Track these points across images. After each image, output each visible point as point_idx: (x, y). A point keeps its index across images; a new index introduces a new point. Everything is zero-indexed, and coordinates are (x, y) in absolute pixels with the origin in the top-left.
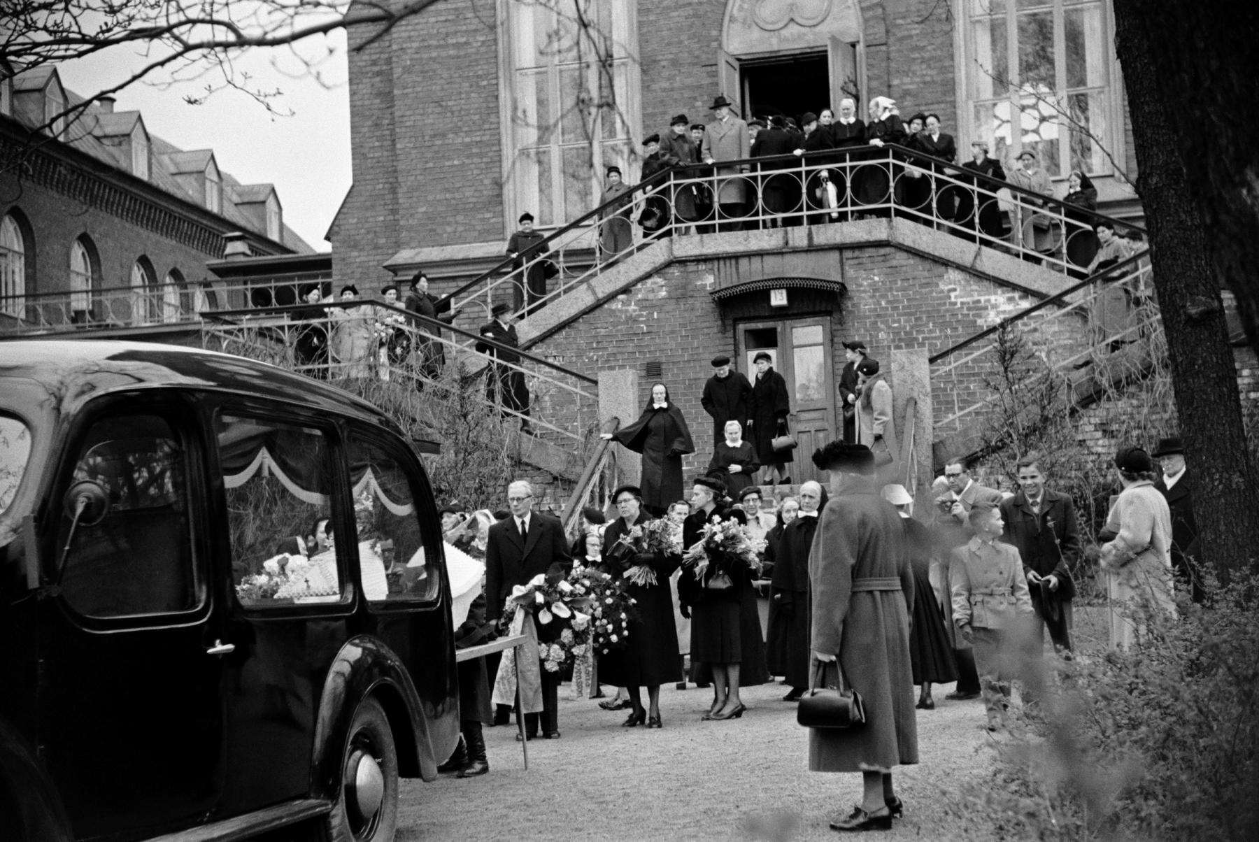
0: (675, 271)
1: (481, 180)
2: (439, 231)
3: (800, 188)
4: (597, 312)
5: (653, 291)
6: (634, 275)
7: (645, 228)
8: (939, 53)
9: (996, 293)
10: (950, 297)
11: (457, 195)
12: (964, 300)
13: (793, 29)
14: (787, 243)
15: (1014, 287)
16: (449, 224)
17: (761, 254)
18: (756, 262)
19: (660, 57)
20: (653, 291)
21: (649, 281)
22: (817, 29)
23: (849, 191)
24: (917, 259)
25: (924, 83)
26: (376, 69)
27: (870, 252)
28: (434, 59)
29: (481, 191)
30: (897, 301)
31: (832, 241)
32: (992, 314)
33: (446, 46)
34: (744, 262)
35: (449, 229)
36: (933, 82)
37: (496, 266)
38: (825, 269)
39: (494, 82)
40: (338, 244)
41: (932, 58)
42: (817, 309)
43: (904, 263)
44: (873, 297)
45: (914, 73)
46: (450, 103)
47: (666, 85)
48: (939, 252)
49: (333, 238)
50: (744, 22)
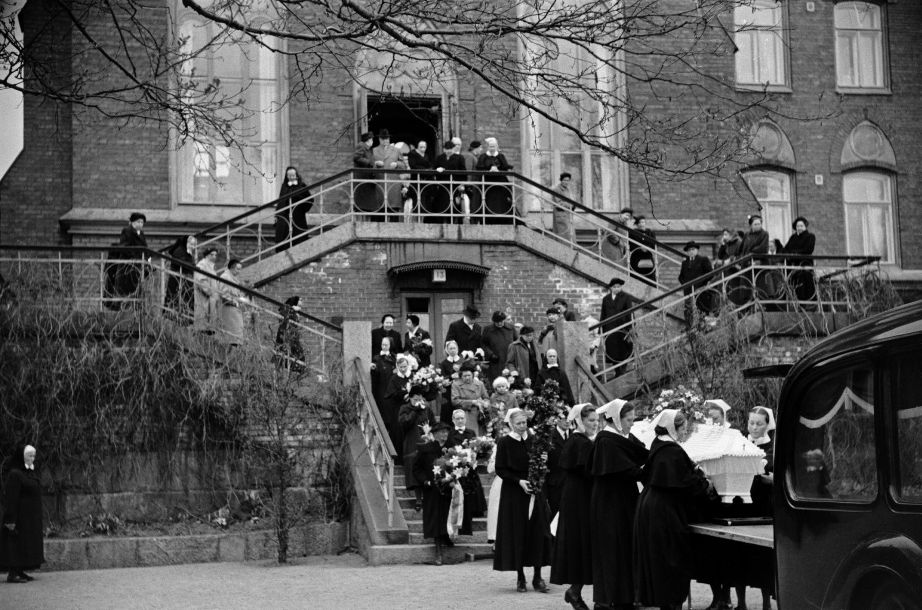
0: (357, 248)
1: (151, 160)
3: (449, 197)
4: (293, 275)
5: (338, 262)
6: (324, 248)
7: (635, 218)
9: (587, 287)
11: (127, 169)
14: (442, 236)
16: (120, 191)
17: (423, 242)
18: (419, 247)
20: (338, 262)
21: (336, 255)
23: (484, 203)
24: (534, 258)
25: (500, 132)
27: (501, 248)
29: (149, 168)
30: (520, 286)
32: (584, 301)
34: (410, 247)
35: (119, 196)
36: (506, 132)
37: (202, 230)
38: (471, 256)
43: (525, 259)
45: (493, 124)
48: (550, 254)
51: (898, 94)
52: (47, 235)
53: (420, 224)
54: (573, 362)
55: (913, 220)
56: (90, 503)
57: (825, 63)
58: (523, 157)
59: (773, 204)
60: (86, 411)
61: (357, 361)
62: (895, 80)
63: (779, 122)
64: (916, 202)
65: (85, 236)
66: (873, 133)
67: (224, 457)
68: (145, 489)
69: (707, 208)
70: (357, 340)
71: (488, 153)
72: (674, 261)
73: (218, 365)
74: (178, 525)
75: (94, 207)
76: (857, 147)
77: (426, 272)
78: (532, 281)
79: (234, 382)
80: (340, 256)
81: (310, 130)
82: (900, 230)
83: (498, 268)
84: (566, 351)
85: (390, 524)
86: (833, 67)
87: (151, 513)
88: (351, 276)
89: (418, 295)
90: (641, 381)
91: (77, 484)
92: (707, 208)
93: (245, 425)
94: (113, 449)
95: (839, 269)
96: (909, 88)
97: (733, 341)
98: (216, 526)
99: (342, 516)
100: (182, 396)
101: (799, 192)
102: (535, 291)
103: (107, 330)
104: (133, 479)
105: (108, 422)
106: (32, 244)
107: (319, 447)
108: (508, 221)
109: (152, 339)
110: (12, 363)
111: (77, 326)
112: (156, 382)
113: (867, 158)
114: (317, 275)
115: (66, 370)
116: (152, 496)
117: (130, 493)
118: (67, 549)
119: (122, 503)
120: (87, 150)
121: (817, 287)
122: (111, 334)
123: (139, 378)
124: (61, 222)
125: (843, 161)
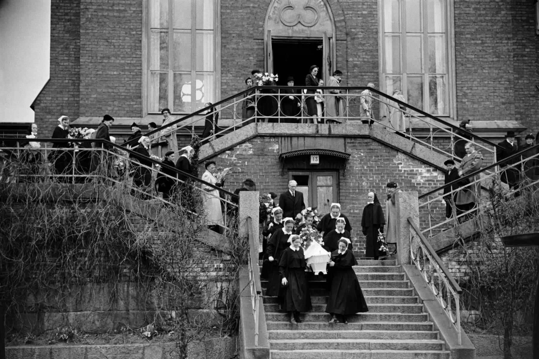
0: (258, 141)
1: (130, 84)
2: (104, 108)
5: (245, 150)
6: (236, 141)
8: (371, 48)
9: (421, 167)
10: (398, 167)
11: (115, 91)
12: (405, 169)
13: (300, 27)
14: (318, 132)
15: (431, 165)
16: (110, 106)
17: (304, 136)
18: (301, 140)
19: (231, 32)
20: (245, 150)
21: (244, 145)
22: (312, 28)
24: (383, 146)
25: (364, 61)
26: (67, 17)
27: (360, 140)
28: (105, 17)
31: (341, 133)
32: (419, 177)
33: (113, 10)
34: (295, 140)
35: (109, 108)
36: (368, 62)
38: (337, 146)
39: (139, 33)
40: (38, 110)
41: (367, 50)
42: (332, 167)
43: (376, 147)
44: (360, 163)
45: (359, 56)
46: (114, 41)
47: (235, 46)
49: (36, 107)
50: (275, 20)
54: (406, 222)
58: (380, 78)
61: (249, 220)
68: (99, 309)
69: (513, 112)
72: (487, 149)
73: (151, 221)
74: (118, 336)
75: (92, 116)
78: (381, 163)
80: (247, 146)
81: (235, 63)
83: (357, 154)
84: (401, 213)
85: (256, 343)
87: (103, 326)
88: (254, 160)
89: (301, 173)
90: (458, 236)
92: (513, 112)
97: (529, 207)
99: (233, 331)
100: (125, 244)
103: (75, 197)
104: (91, 301)
107: (222, 281)
110: (8, 219)
114: (231, 160)
116: (104, 314)
117: (89, 312)
119: (82, 319)
120: (89, 78)
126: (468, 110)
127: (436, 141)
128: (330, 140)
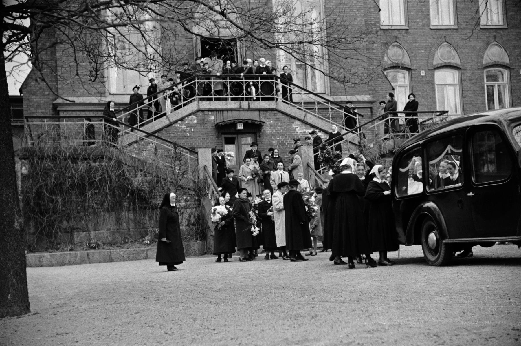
0: (200, 114)
4: (170, 127)
5: (191, 121)
6: (184, 114)
14: (241, 107)
17: (232, 110)
18: (230, 112)
21: (190, 117)
27: (269, 112)
34: (225, 112)
38: (254, 116)
51: (461, 28)
52: (47, 111)
53: (229, 101)
55: (469, 92)
56: (86, 236)
57: (425, 14)
59: (400, 86)
60: (83, 193)
62: (459, 21)
63: (403, 45)
64: (470, 83)
65: (66, 111)
66: (449, 49)
67: (146, 214)
70: (205, 158)
71: (261, 66)
74: (127, 245)
76: (441, 56)
77: (234, 124)
79: (149, 178)
82: (463, 97)
86: (429, 15)
89: (230, 136)
91: (79, 227)
92: (367, 90)
93: (154, 198)
94: (95, 211)
95: (430, 117)
96: (466, 25)
98: (145, 244)
101: (413, 79)
102: (286, 132)
103: (89, 156)
105: (92, 198)
106: (39, 116)
108: (272, 99)
109: (110, 159)
111: (75, 154)
112: (113, 179)
113: (446, 61)
115: (72, 174)
118: (79, 256)
119: (100, 236)
121: (419, 126)
122: (91, 157)
123: (105, 178)
124: (53, 104)
125: (434, 63)
126: (338, 89)
127: (320, 111)
128: (249, 112)
